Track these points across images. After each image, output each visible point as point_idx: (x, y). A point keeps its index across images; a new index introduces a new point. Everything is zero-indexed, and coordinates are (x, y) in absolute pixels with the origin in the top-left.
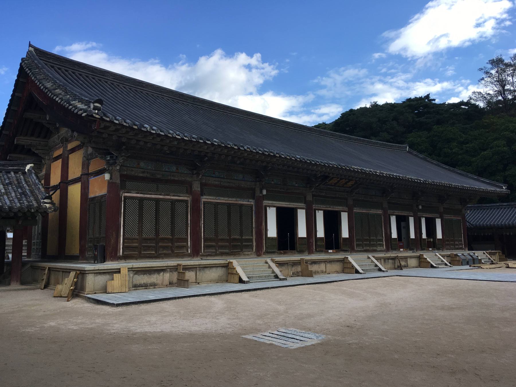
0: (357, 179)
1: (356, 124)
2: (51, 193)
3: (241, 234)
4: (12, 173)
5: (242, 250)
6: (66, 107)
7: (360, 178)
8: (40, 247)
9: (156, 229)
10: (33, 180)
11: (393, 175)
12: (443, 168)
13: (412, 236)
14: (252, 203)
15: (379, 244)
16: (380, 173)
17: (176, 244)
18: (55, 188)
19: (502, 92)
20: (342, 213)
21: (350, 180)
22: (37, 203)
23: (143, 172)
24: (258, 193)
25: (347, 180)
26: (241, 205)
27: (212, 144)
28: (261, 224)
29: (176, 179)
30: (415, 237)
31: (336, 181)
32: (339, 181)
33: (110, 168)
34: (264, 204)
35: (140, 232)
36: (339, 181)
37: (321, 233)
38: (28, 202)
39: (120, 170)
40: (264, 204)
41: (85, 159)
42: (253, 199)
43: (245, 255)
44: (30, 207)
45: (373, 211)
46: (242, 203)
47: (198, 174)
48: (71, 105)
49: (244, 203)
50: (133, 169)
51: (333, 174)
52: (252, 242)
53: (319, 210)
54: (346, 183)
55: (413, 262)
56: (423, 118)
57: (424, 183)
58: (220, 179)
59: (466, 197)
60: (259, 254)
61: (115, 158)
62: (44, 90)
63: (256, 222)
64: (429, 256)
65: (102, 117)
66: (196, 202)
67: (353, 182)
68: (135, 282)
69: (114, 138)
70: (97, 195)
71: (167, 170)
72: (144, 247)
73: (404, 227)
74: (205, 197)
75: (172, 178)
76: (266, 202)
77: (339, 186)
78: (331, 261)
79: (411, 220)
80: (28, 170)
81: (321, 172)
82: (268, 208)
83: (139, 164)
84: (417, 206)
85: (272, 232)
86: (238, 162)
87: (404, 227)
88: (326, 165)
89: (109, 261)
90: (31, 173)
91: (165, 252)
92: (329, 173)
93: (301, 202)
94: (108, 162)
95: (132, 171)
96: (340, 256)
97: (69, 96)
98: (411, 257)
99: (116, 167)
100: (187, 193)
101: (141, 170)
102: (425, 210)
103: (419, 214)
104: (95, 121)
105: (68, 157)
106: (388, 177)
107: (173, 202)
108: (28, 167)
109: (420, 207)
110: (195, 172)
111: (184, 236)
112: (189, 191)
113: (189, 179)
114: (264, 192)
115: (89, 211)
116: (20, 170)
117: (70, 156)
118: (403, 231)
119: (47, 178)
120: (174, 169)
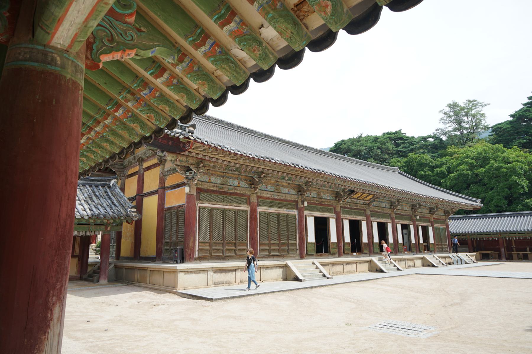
0: (375, 193)
3: (288, 239)
5: (289, 253)
8: (115, 250)
9: (223, 234)
12: (428, 186)
13: (413, 241)
14: (296, 213)
17: (239, 248)
19: (460, 128)
20: (363, 222)
24: (300, 205)
26: (287, 215)
28: (303, 231)
29: (238, 192)
33: (189, 182)
34: (305, 214)
35: (211, 238)
37: (347, 239)
40: (305, 214)
41: (162, 175)
42: (296, 209)
43: (291, 257)
46: (288, 212)
49: (290, 213)
50: (206, 184)
52: (296, 246)
53: (345, 219)
54: (366, 197)
55: (419, 263)
56: (400, 147)
58: (271, 193)
60: (302, 257)
61: (193, 174)
63: (299, 229)
64: (429, 257)
67: (372, 196)
68: (214, 281)
70: (174, 205)
71: (231, 184)
72: (214, 249)
75: (236, 191)
76: (306, 212)
78: (361, 262)
82: (308, 217)
84: (416, 216)
85: (311, 237)
89: (188, 261)
91: (230, 254)
93: (331, 212)
95: (205, 185)
96: (281, 262)
98: (417, 259)
100: (246, 203)
101: (213, 184)
102: (374, 214)
103: (417, 223)
105: (143, 174)
107: (236, 212)
108: (113, 182)
109: (418, 217)
110: (253, 186)
111: (245, 242)
112: (296, 207)
114: (306, 204)
115: (165, 219)
116: (106, 184)
117: (145, 173)
120: (236, 183)
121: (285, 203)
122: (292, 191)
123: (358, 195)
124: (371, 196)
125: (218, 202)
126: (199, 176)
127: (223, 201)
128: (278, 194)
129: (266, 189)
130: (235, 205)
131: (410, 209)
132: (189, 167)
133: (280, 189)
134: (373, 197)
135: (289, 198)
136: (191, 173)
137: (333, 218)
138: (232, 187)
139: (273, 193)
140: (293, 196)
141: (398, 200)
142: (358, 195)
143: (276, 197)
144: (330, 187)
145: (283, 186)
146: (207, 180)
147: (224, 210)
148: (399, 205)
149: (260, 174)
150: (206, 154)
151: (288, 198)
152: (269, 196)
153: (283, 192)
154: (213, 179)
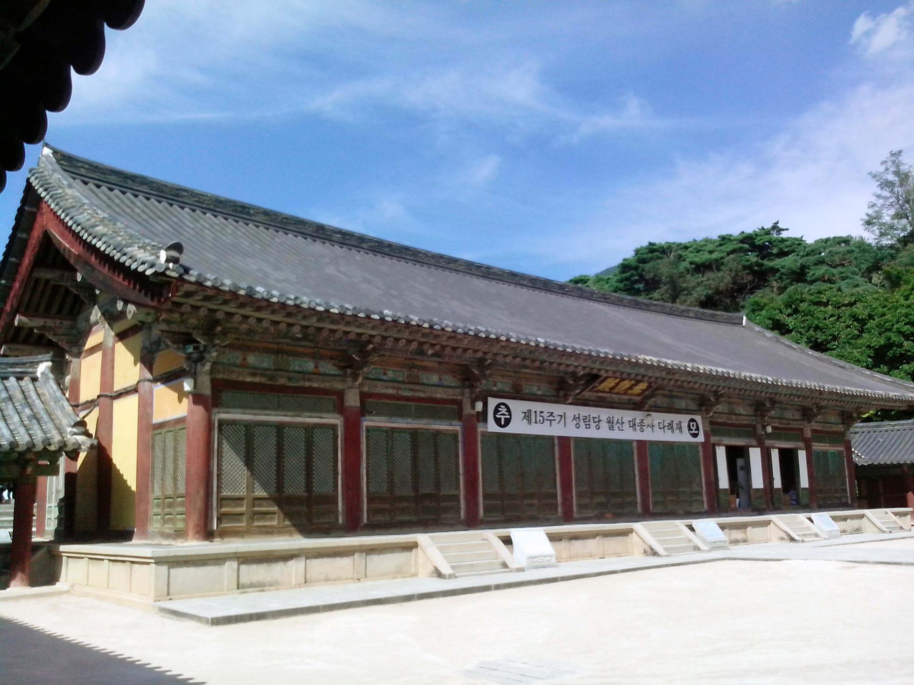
0: (653, 380)
1: (644, 279)
2: (82, 414)
4: (12, 380)
6: (116, 258)
7: (657, 378)
10: (51, 392)
11: (666, 364)
12: (835, 364)
14: (458, 428)
15: (695, 501)
16: (693, 368)
18: (91, 404)
21: (638, 382)
22: (61, 434)
23: (254, 375)
24: (467, 410)
25: (633, 382)
26: (438, 433)
27: (382, 320)
30: (810, 485)
31: (613, 384)
32: (617, 384)
35: (416, 488)
36: (617, 384)
37: (778, 483)
38: (44, 433)
39: (212, 371)
42: (460, 419)
44: (47, 442)
45: (443, 426)
47: (355, 377)
48: (125, 254)
50: (235, 369)
51: (607, 371)
54: (631, 388)
57: (774, 386)
58: (396, 385)
59: (851, 411)
62: (73, 228)
65: (181, 276)
66: (352, 429)
69: (203, 312)
71: (297, 368)
73: (742, 468)
74: (368, 418)
75: (307, 384)
77: (618, 393)
79: (755, 455)
80: (42, 374)
81: (584, 368)
83: (245, 359)
84: (764, 428)
86: (430, 352)
87: (742, 468)
88: (593, 354)
90: (48, 379)
92: (599, 370)
94: (189, 357)
95: (232, 372)
97: (120, 238)
99: (203, 365)
102: (779, 433)
103: (768, 442)
104: (169, 283)
106: (709, 376)
107: (310, 429)
110: (349, 371)
112: (459, 414)
113: (339, 386)
114: (769, 429)
118: (741, 474)
119: (75, 387)
120: (310, 366)
121: (432, 407)
122: (449, 380)
123: (610, 383)
124: (643, 386)
125: (265, 408)
126: (214, 354)
127: (279, 407)
128: (413, 387)
129: (384, 377)
130: (308, 414)
131: (750, 411)
132: (189, 334)
133: (417, 376)
134: (649, 387)
135: (440, 394)
136: (195, 348)
137: (801, 449)
138: (300, 376)
139: (403, 386)
140: (450, 391)
141: (716, 392)
142: (610, 383)
143: (409, 394)
144: (539, 368)
145: (425, 369)
146: (238, 362)
147: (280, 428)
148: (819, 414)
149: (360, 344)
150: (214, 307)
151: (438, 396)
152: (390, 391)
153: (425, 381)
154: (252, 359)
